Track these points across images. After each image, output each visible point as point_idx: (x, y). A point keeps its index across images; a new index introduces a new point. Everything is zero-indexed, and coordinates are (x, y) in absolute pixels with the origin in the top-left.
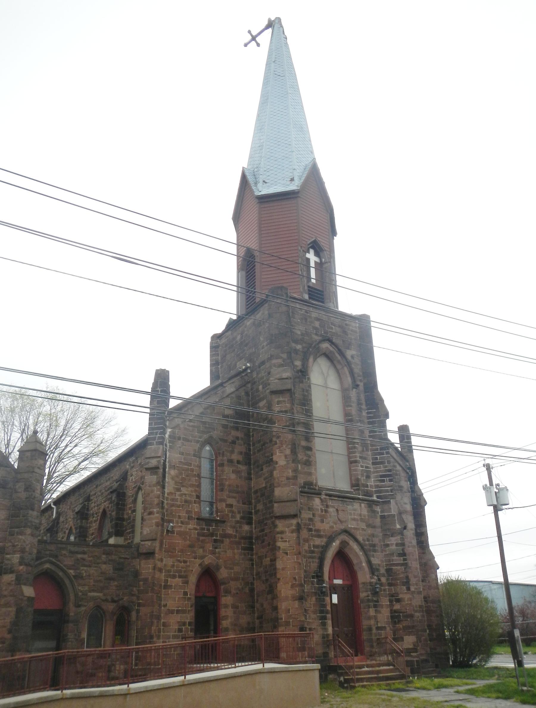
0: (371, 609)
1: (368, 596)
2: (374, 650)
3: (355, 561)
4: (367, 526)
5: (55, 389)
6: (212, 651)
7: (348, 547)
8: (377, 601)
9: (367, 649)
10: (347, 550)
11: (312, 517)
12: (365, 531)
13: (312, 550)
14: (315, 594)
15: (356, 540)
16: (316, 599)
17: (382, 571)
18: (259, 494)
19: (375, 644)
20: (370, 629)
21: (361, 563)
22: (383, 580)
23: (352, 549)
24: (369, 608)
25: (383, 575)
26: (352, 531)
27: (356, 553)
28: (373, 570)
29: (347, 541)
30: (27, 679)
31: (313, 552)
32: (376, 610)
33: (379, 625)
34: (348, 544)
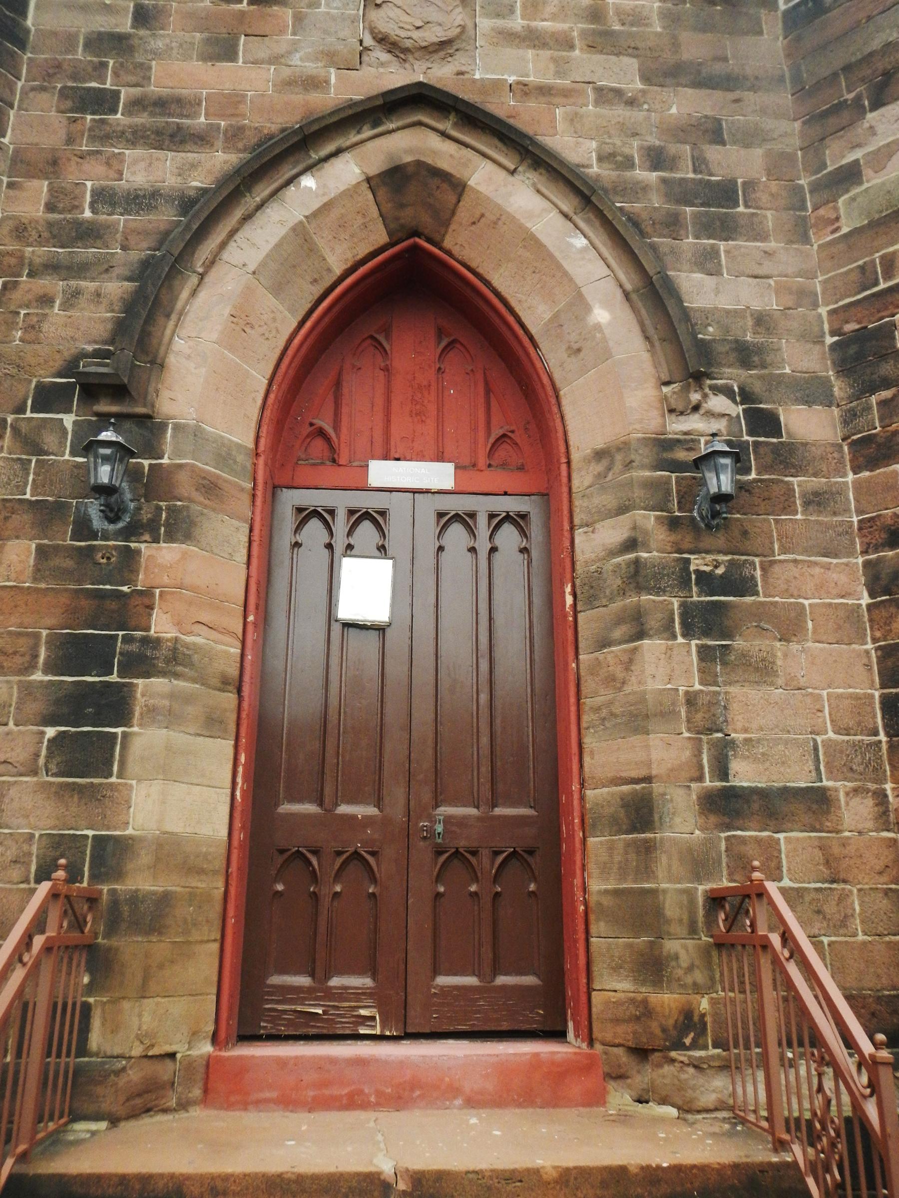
0: (652, 646)
1: (631, 544)
2: (667, 1000)
3: (535, 312)
4: (646, 78)
5: (172, 395)
6: (479, 965)
7: (463, 214)
8: (738, 583)
9: (613, 987)
10: (462, 244)
11: (125, 25)
12: (631, 103)
13: (78, 224)
14: (46, 514)
15: (526, 151)
16: (42, 553)
17: (801, 356)
18: (788, 622)
19: (681, 948)
20: (640, 813)
21: (579, 304)
22: (809, 424)
23: (494, 220)
24: (641, 635)
25: (812, 392)
26: (502, 106)
27: (532, 242)
28: (691, 357)
29: (444, 164)
30: (735, 972)
31: (88, 233)
32: (705, 654)
33: (745, 774)
34: (459, 187)
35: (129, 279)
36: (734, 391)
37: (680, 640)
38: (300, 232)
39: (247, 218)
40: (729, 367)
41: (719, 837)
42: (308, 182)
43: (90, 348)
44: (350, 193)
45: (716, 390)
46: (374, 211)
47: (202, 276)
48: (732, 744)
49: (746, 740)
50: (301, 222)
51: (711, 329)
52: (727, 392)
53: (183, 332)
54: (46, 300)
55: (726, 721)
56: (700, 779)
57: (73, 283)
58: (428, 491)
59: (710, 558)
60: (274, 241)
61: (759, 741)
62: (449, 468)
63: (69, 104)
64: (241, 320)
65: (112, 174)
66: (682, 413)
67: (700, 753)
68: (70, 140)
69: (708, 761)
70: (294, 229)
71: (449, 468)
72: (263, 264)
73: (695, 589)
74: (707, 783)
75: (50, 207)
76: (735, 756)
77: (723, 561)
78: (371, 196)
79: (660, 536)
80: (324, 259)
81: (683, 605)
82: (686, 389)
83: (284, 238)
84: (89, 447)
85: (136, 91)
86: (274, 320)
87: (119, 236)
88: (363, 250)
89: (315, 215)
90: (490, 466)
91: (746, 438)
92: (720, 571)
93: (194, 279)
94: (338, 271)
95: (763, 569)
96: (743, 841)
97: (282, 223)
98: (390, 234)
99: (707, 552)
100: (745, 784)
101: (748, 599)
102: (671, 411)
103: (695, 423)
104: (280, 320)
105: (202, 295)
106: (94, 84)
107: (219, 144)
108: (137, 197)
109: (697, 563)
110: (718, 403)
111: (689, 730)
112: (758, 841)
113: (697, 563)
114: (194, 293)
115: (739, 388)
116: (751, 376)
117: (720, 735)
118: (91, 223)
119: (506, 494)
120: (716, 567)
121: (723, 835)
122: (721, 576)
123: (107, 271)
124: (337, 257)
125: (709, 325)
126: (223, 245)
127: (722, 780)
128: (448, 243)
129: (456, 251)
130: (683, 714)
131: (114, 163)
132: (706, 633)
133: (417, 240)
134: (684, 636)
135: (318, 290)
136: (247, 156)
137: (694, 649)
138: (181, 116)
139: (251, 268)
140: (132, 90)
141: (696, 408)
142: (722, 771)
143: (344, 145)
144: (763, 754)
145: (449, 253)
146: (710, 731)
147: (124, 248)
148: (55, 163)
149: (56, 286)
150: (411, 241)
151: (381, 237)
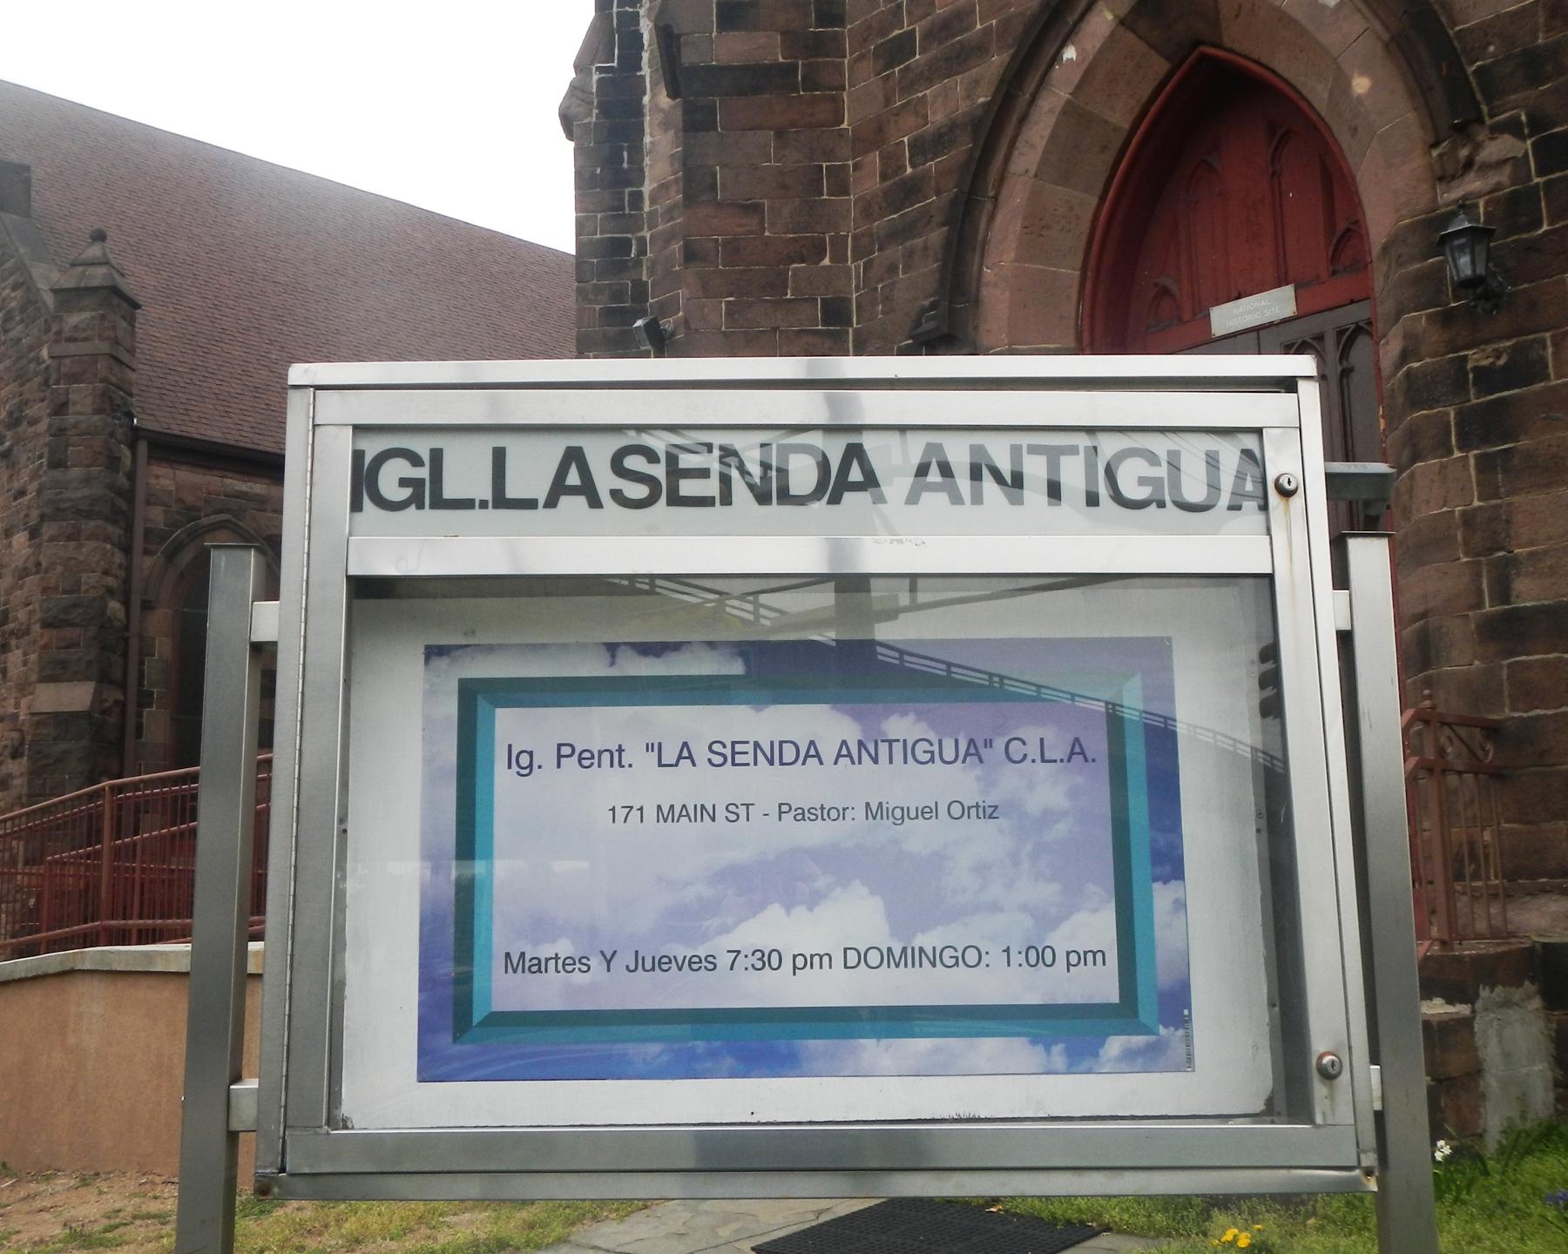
32: (1484, 464)
35: (944, 224)
36: (1520, 122)
37: (1457, 454)
38: (1071, 111)
39: (1023, 119)
40: (1515, 91)
41: (1501, 667)
42: (1070, 53)
43: (926, 303)
44: (1111, 41)
45: (1498, 130)
46: (1141, 47)
47: (996, 198)
48: (1512, 562)
49: (1531, 554)
50: (1068, 102)
51: (1492, 48)
52: (1513, 128)
53: (989, 261)
54: (892, 269)
55: (1508, 536)
56: (1480, 605)
57: (907, 244)
58: (1271, 324)
59: (1489, 348)
60: (1047, 133)
61: (1545, 552)
62: (1288, 291)
63: (881, 63)
64: (1036, 225)
65: (920, 121)
66: (1453, 177)
67: (1478, 576)
68: (888, 101)
69: (1489, 583)
70: (1064, 112)
71: (1288, 291)
72: (1043, 162)
73: (1472, 391)
74: (1488, 608)
75: (884, 177)
76: (1518, 575)
77: (1505, 349)
78: (1131, 36)
79: (1434, 337)
80: (1106, 122)
81: (1459, 413)
82: (1454, 148)
83: (1056, 125)
84: (63, 876)
85: (925, 22)
86: (1071, 209)
87: (933, 183)
88: (1146, 91)
89: (1079, 87)
90: (1334, 273)
91: (1537, 180)
92: (1502, 362)
93: (989, 206)
94: (1126, 126)
95: (1555, 344)
96: (1527, 666)
97: (1051, 110)
98: (1168, 59)
99: (1487, 342)
100: (1528, 604)
101: (1538, 386)
102: (1441, 179)
103: (1473, 184)
104: (1080, 204)
105: (999, 218)
106: (897, 32)
107: (993, 47)
108: (940, 136)
109: (1477, 358)
110: (1498, 147)
111: (1466, 555)
112: (1545, 664)
113: (1477, 358)
114: (992, 218)
115: (1527, 115)
116: (1543, 93)
117: (1501, 554)
118: (912, 177)
119: (1352, 302)
120: (1498, 358)
121: (1505, 662)
122: (1504, 367)
123: (929, 222)
124: (1119, 115)
125: (1489, 44)
126: (1007, 159)
127: (1503, 603)
128: (1227, 42)
129: (1236, 47)
130: (1460, 537)
131: (919, 108)
132: (1486, 441)
133: (1203, 48)
134: (1461, 449)
135: (1109, 157)
136: (1012, 51)
137: (1472, 461)
138: (961, 32)
139: (1032, 172)
140: (923, 22)
141: (1469, 164)
142: (1503, 592)
143: (632, 433)
144: (1551, 567)
145: (1232, 51)
146: (1491, 550)
147: (938, 193)
148: (880, 130)
149: (896, 252)
150: (1195, 54)
151: (1160, 66)
